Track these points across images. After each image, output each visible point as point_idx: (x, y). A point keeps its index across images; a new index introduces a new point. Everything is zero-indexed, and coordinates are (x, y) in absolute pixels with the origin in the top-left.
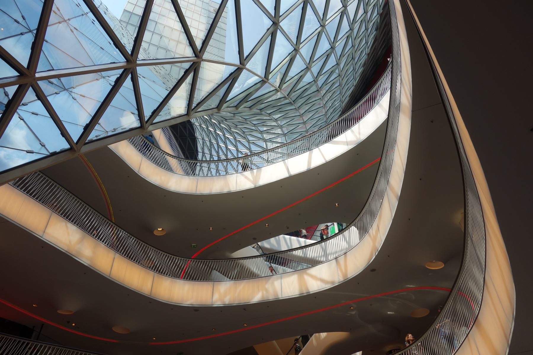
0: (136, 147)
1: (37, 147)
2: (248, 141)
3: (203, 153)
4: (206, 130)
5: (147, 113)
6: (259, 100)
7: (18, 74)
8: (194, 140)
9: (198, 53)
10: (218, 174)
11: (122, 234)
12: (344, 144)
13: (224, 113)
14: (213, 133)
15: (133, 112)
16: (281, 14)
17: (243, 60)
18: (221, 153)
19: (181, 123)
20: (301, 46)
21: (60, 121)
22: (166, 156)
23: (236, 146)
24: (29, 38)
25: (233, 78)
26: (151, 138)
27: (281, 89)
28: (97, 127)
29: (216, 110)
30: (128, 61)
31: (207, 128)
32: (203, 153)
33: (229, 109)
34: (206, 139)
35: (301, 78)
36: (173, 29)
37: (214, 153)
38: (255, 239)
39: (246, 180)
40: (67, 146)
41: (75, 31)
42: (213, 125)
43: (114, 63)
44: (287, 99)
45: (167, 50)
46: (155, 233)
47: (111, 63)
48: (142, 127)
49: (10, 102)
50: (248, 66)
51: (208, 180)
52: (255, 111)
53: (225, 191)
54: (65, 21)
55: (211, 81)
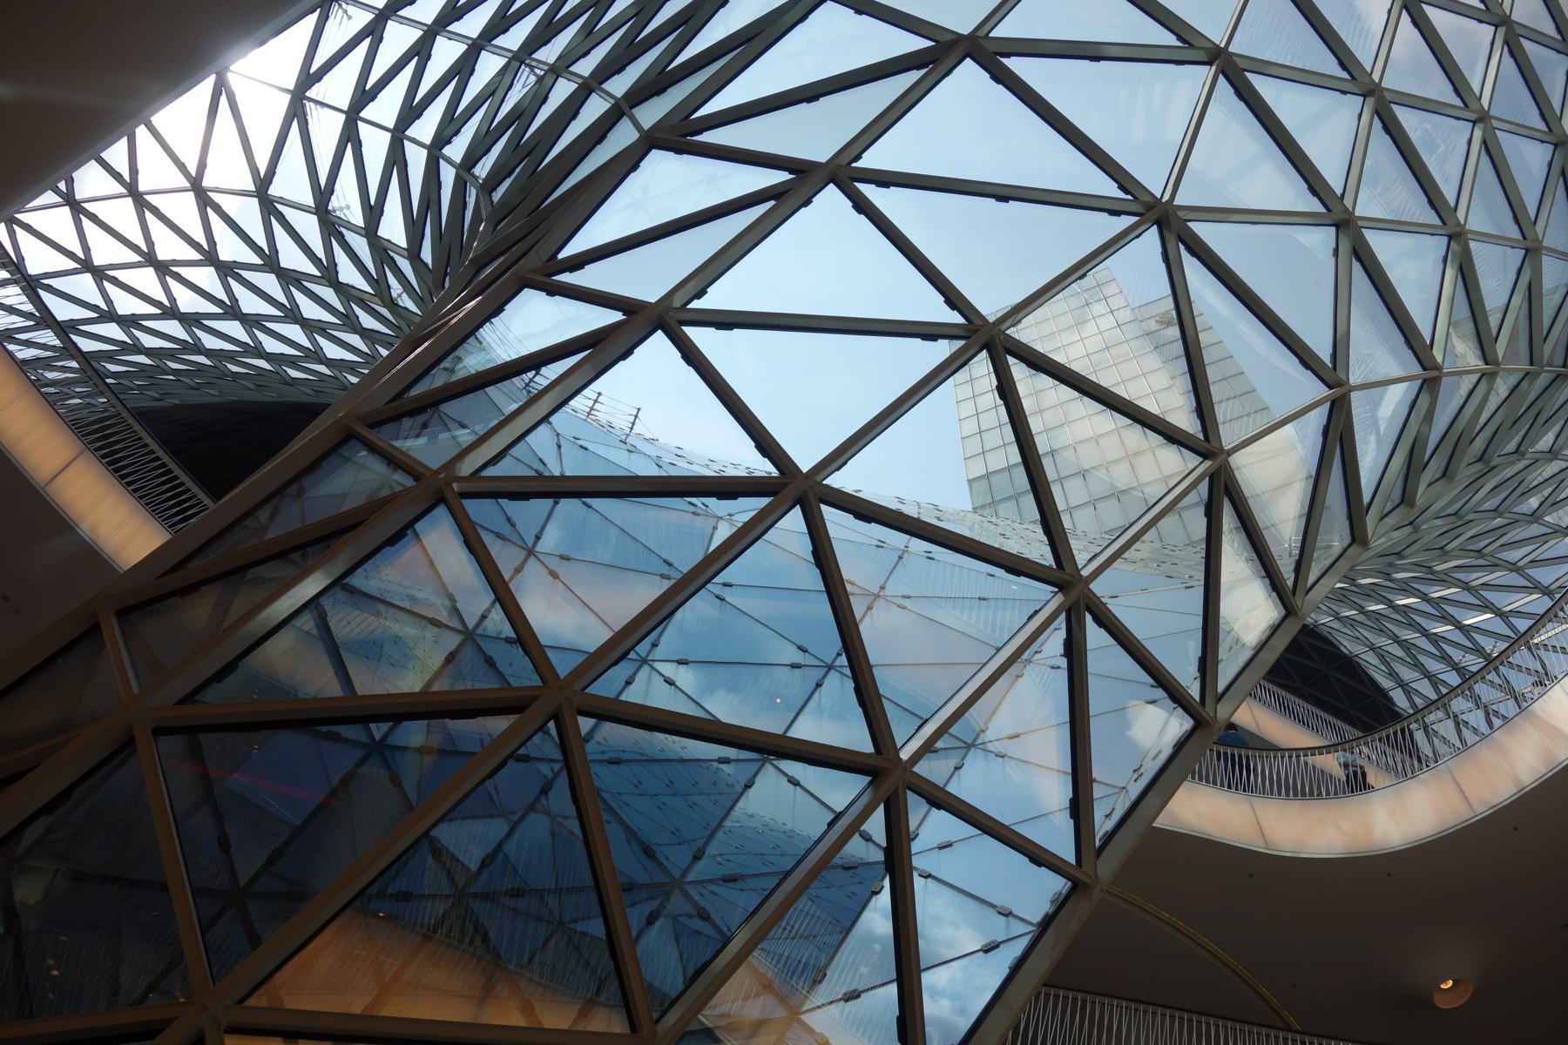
0: (1215, 783)
1: (999, 928)
2: (1514, 567)
3: (1403, 685)
4: (1361, 618)
5: (1187, 676)
6: (1456, 440)
7: (868, 779)
8: (1350, 666)
9: (1205, 444)
10: (1497, 722)
13: (1382, 540)
14: (1389, 612)
15: (1151, 698)
16: (1339, 192)
17: (1330, 373)
18: (1456, 655)
19: (1287, 650)
20: (1461, 214)
21: (1007, 828)
22: (1310, 759)
23: (1486, 607)
24: (840, 688)
25: (1338, 438)
26: (1234, 736)
27: (1496, 363)
28: (1098, 791)
29: (1354, 548)
30: (1061, 587)
31: (1362, 610)
32: (1403, 685)
33: (1390, 521)
34: (1382, 641)
36: (1096, 439)
37: (1433, 666)
40: (1059, 884)
41: (906, 603)
42: (1372, 593)
43: (1036, 612)
44: (1537, 375)
45: (1118, 495)
46: (1442, 1003)
48: (1200, 723)
49: (889, 851)
50: (1354, 379)
51: (1484, 752)
52: (1465, 472)
54: (878, 596)
55: (1289, 484)
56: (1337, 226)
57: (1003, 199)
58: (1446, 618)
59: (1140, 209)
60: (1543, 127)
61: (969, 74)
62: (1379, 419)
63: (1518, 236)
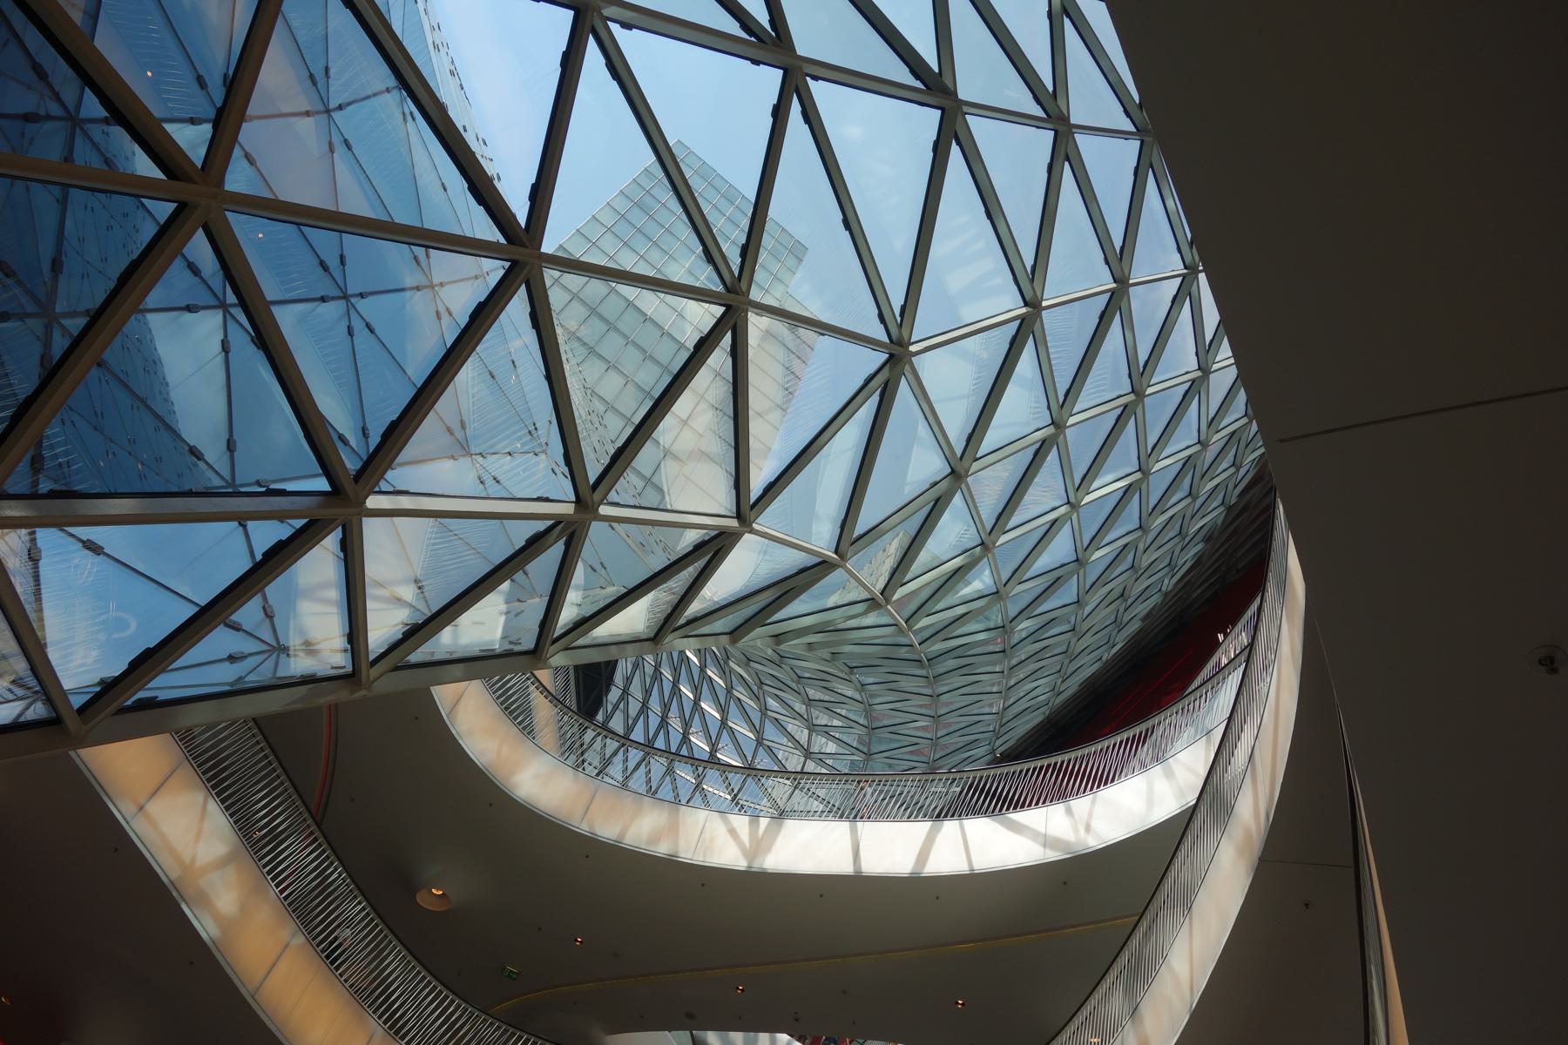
2: (764, 710)
3: (625, 692)
11: (336, 874)
12: (1034, 840)
23: (723, 710)
32: (625, 692)
35: (958, 574)
37: (655, 705)
38: (690, 1016)
39: (729, 837)
43: (547, 500)
44: (922, 666)
47: (539, 499)
53: (662, 849)
56: (953, 471)
57: (847, 225)
58: (696, 690)
59: (894, 336)
60: (1086, 543)
61: (930, 119)
62: (833, 593)
63: (1004, 580)
